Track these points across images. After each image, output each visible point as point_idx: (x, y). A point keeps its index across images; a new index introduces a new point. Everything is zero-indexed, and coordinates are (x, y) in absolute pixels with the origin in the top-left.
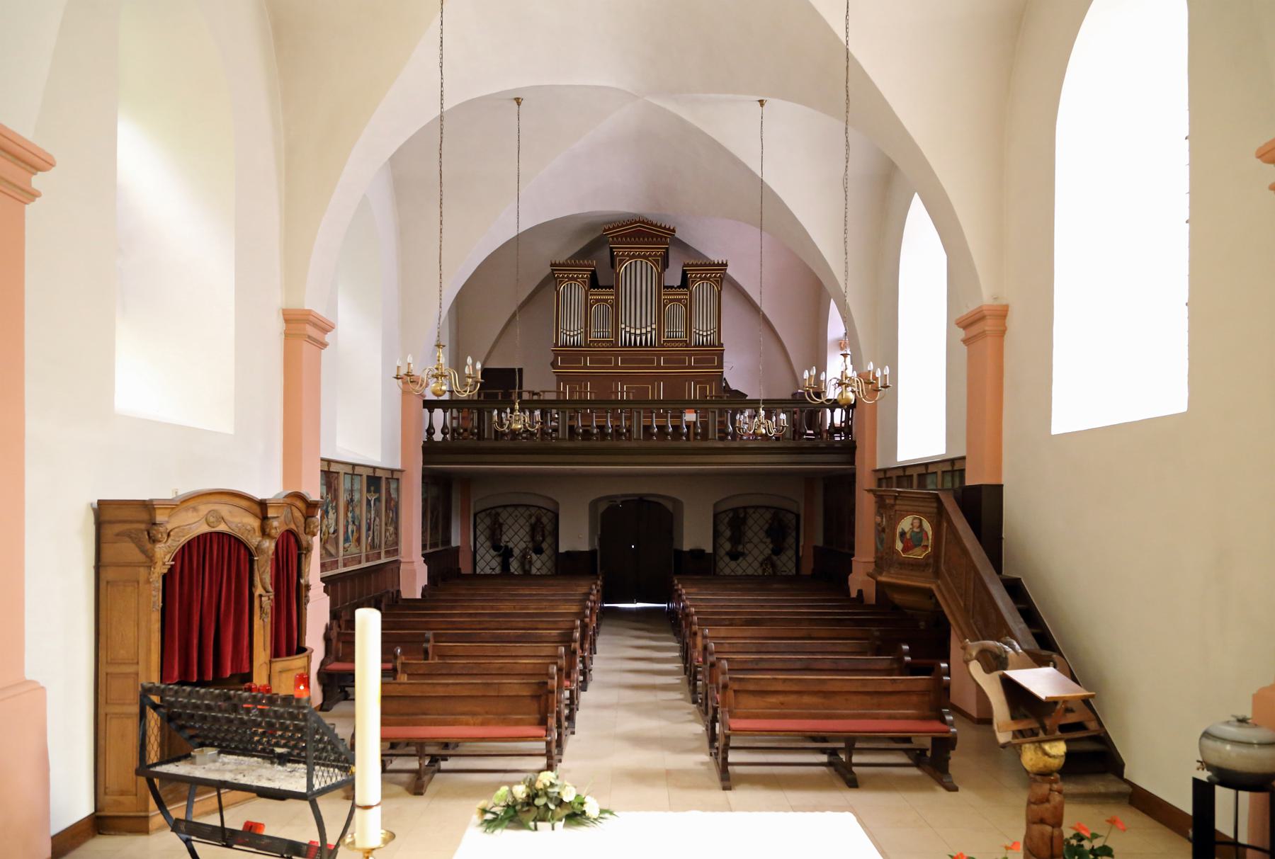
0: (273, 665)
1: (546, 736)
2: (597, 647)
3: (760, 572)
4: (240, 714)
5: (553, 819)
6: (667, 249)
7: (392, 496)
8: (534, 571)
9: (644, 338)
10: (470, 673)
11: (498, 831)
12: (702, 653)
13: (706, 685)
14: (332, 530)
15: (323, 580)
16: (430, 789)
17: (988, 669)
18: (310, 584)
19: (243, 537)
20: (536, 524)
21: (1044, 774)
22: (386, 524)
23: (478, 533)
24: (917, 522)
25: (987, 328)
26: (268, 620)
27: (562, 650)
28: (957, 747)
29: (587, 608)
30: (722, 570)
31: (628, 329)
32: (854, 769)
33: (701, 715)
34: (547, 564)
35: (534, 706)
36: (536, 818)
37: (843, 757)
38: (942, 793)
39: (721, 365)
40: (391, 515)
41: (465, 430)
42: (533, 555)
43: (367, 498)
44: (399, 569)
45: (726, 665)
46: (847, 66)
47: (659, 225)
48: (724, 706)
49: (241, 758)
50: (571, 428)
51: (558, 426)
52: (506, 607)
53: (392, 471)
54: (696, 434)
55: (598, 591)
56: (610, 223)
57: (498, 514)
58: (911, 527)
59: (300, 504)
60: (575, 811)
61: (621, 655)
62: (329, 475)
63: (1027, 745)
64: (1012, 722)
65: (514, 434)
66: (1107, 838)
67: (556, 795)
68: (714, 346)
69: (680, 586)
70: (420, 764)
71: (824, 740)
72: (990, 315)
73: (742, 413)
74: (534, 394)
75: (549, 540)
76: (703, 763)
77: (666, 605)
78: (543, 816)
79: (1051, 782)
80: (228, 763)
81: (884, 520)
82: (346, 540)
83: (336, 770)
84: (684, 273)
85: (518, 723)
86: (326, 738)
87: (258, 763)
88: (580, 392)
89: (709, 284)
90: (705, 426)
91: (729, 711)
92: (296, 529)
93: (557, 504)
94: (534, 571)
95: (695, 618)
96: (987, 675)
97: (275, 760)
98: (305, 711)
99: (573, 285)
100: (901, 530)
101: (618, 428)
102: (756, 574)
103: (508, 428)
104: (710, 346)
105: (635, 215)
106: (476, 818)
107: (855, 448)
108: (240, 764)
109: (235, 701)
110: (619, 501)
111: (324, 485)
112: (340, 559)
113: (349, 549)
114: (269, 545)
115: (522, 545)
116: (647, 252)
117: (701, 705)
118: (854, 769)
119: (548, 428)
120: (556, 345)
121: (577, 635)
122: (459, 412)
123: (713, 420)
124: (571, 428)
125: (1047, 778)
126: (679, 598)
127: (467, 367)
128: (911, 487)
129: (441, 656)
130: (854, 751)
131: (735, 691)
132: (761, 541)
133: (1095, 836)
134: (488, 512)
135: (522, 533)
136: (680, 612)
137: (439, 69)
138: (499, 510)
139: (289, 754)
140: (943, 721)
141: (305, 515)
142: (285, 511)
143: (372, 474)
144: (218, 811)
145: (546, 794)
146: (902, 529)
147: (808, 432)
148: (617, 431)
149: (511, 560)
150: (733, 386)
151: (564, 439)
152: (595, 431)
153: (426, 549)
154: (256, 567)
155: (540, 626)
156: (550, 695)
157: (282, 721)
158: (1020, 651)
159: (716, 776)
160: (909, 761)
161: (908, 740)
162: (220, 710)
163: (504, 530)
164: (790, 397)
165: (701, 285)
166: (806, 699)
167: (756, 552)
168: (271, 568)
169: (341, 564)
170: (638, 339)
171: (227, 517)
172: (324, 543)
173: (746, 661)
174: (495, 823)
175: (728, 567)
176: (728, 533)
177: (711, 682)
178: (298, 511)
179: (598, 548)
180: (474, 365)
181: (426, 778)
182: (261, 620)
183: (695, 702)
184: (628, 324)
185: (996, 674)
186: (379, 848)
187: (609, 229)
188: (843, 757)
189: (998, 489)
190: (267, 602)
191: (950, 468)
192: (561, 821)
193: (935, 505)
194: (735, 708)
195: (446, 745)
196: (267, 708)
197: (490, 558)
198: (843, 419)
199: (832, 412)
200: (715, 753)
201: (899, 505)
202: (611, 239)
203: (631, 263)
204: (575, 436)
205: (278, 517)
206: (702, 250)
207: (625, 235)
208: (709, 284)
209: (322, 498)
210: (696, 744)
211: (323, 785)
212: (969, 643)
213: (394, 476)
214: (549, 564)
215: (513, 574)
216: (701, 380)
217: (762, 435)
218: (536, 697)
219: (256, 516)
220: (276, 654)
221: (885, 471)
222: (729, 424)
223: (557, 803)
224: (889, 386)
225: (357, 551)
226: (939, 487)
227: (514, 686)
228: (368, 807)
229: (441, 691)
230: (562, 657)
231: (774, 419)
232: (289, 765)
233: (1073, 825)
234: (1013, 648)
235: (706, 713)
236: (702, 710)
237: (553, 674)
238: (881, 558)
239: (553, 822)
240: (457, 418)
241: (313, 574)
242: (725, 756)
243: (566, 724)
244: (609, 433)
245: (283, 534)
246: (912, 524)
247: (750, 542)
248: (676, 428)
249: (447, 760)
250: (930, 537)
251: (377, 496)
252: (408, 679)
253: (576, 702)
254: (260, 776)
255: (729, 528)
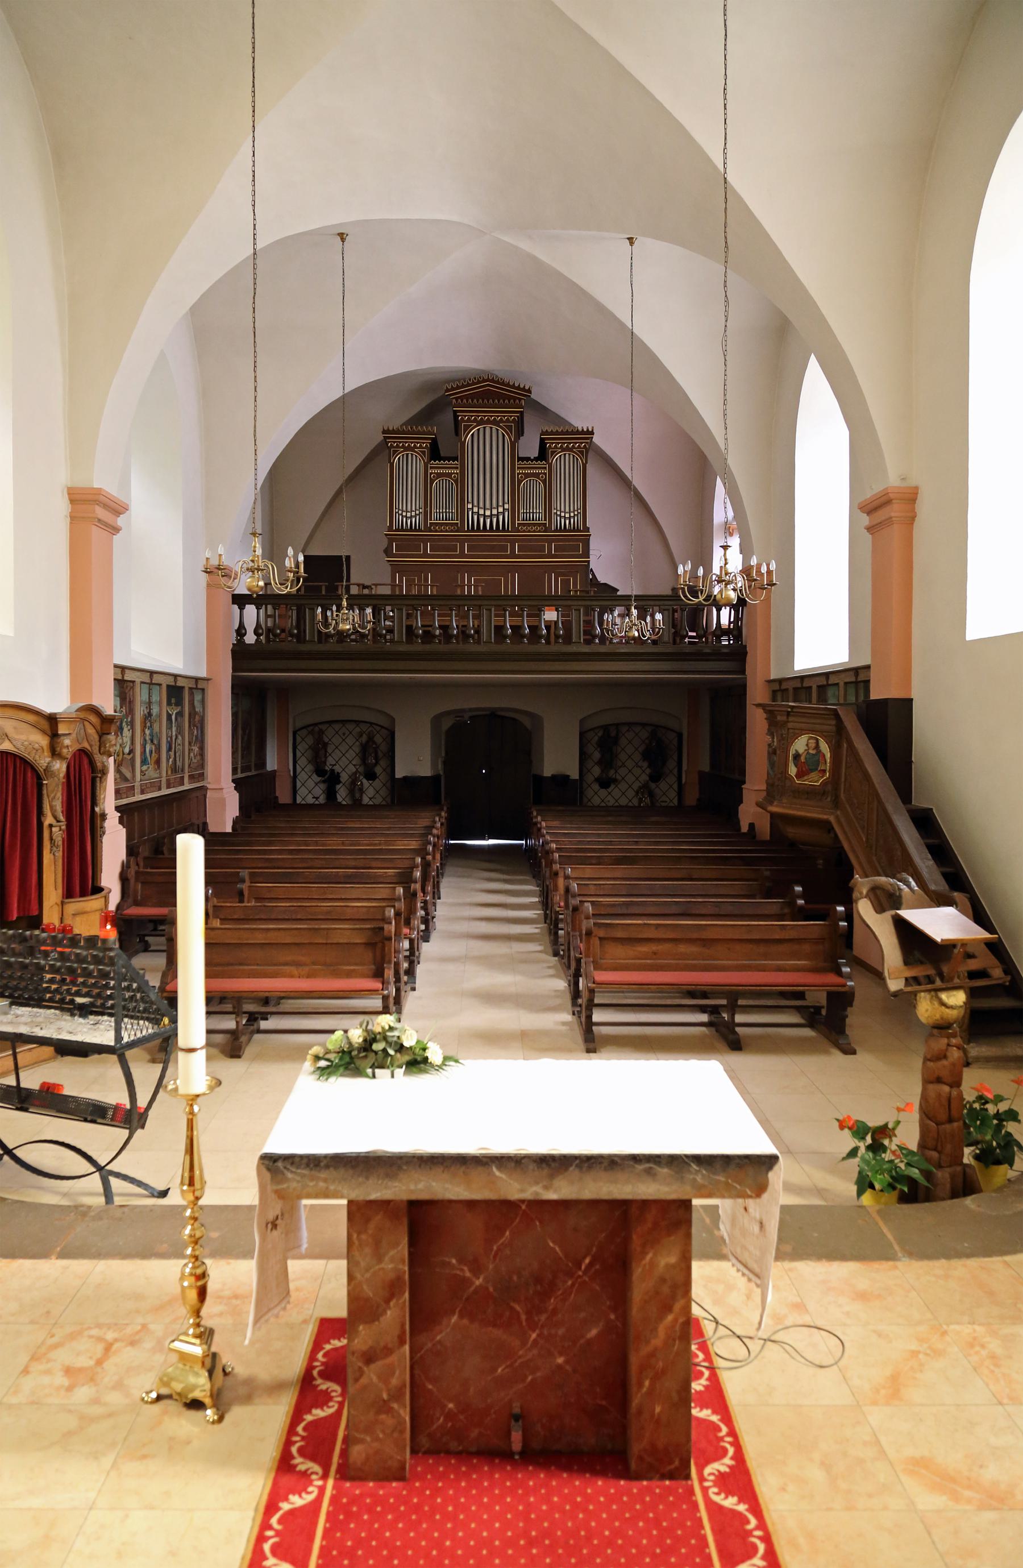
0: (66, 907)
1: (382, 990)
2: (442, 891)
3: (635, 802)
4: (37, 958)
5: (392, 1066)
6: (522, 413)
7: (197, 710)
8: (366, 800)
9: (495, 520)
10: (294, 917)
11: (332, 1079)
12: (563, 898)
13: (569, 933)
14: (127, 750)
15: (118, 809)
16: (249, 1051)
17: (880, 909)
18: (106, 812)
19: (30, 757)
20: (367, 742)
21: (941, 1027)
22: (190, 744)
23: (298, 754)
24: (812, 743)
25: (893, 514)
26: (59, 854)
27: (400, 891)
28: (856, 1002)
29: (430, 843)
30: (589, 800)
31: (475, 510)
32: (738, 1029)
33: (562, 968)
34: (381, 792)
35: (368, 955)
36: (374, 1064)
37: (725, 1016)
38: (838, 1058)
39: (586, 553)
40: (195, 732)
41: (283, 631)
42: (365, 781)
43: (167, 711)
44: (205, 796)
45: (590, 908)
46: (726, 208)
47: (511, 384)
48: (587, 956)
49: (35, 1010)
50: (409, 628)
51: (394, 626)
52: (334, 843)
53: (197, 680)
54: (557, 637)
55: (442, 824)
56: (453, 381)
57: (321, 732)
58: (806, 748)
59: (93, 719)
60: (416, 1057)
61: (468, 900)
62: (124, 685)
63: (923, 994)
64: (905, 967)
65: (342, 635)
66: (1013, 1101)
67: (395, 1039)
68: (578, 530)
69: (539, 818)
70: (237, 1022)
71: (705, 995)
72: (896, 499)
73: (612, 611)
74: (365, 587)
75: (383, 763)
76: (564, 1024)
77: (524, 842)
78: (382, 1062)
79: (949, 1036)
80: (22, 1016)
81: (775, 740)
82: (144, 762)
83: (147, 1023)
84: (542, 443)
85: (349, 975)
86: (135, 985)
87: (56, 1015)
88: (420, 586)
89: (571, 456)
90: (567, 626)
91: (593, 962)
92: (89, 748)
93: (393, 720)
94: (366, 800)
95: (556, 855)
96: (878, 916)
97: (76, 1012)
98: (112, 954)
99: (410, 455)
100: (794, 752)
101: (464, 629)
102: (630, 804)
103: (334, 629)
104: (574, 530)
105: (483, 371)
106: (308, 1065)
107: (744, 654)
108: (35, 1016)
109: (32, 943)
110: (466, 716)
111: (117, 696)
112: (137, 785)
113: (146, 772)
114: (60, 767)
115: (352, 769)
116: (498, 416)
117: (562, 957)
118: (738, 1029)
119: (382, 629)
120: (390, 528)
121: (418, 874)
122: (275, 609)
123: (578, 619)
124: (409, 628)
125: (944, 1032)
126: (539, 834)
127: (287, 559)
128: (810, 702)
129: (258, 899)
130: (737, 1009)
131: (601, 939)
132: (637, 766)
133: (999, 1099)
134: (310, 729)
135: (351, 754)
136: (540, 849)
137: (251, 208)
138: (323, 727)
139: (92, 1004)
140: (840, 973)
141: (100, 732)
142: (78, 726)
143: (173, 684)
144: (14, 1073)
145: (385, 1038)
146: (796, 750)
147: (690, 634)
148: (463, 632)
149: (338, 787)
150: (602, 579)
151: (400, 642)
152: (437, 632)
153: (237, 774)
154: (45, 792)
155: (374, 864)
156: (387, 942)
157: (84, 966)
158: (916, 888)
159: (579, 1038)
160: (802, 1021)
161: (801, 996)
162: (14, 954)
163: (329, 750)
164: (669, 593)
165: (562, 457)
166: (682, 948)
167: (630, 778)
168: (62, 795)
169: (137, 790)
170: (488, 521)
171: (12, 733)
172: (118, 766)
173: (613, 905)
174: (328, 1071)
175: (596, 796)
176: (597, 755)
177: (573, 930)
178: (92, 727)
179: (441, 773)
180: (296, 556)
181: (243, 1039)
182: (52, 855)
183: (556, 954)
184: (475, 503)
185: (888, 915)
186: (204, 1094)
187: (453, 389)
188: (725, 1016)
189: (907, 704)
190: (58, 834)
191: (853, 679)
192: (402, 1068)
193: (834, 722)
194: (601, 959)
195: (266, 1001)
196: (67, 950)
197: (313, 784)
198: (732, 620)
199: (719, 610)
200: (578, 1011)
201: (792, 722)
202: (454, 401)
203: (478, 430)
204: (414, 638)
205: (69, 734)
206: (563, 414)
207: (472, 397)
208: (571, 456)
209: (115, 711)
210: (558, 1001)
211: (132, 1038)
212: (860, 879)
213: (198, 685)
214: (384, 792)
215: (340, 803)
216: (565, 571)
217: (634, 638)
218: (370, 945)
219: (44, 732)
220: (69, 893)
221: (780, 681)
222: (597, 625)
223: (397, 1048)
224: (775, 584)
225: (157, 775)
226: (842, 701)
227: (344, 933)
228: (192, 1050)
229: (260, 938)
230: (400, 900)
231: (648, 619)
232: (91, 1017)
233: (974, 1086)
234: (909, 886)
235: (569, 967)
236: (564, 963)
237: (390, 918)
238: (772, 785)
239: (392, 1069)
240: (273, 616)
241: (108, 802)
242: (588, 1013)
243: (405, 978)
244: (454, 635)
245: (74, 755)
246: (807, 745)
247: (623, 765)
248: (534, 629)
249: (267, 1019)
250: (828, 761)
251: (179, 709)
252: (221, 924)
253: (417, 953)
254: (59, 1029)
255: (599, 749)
